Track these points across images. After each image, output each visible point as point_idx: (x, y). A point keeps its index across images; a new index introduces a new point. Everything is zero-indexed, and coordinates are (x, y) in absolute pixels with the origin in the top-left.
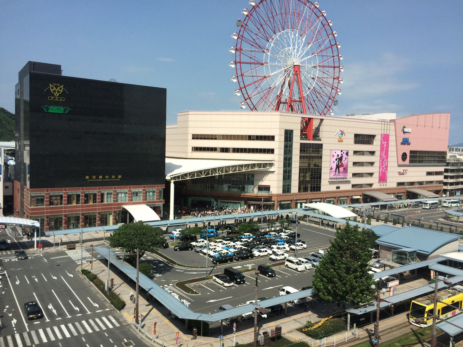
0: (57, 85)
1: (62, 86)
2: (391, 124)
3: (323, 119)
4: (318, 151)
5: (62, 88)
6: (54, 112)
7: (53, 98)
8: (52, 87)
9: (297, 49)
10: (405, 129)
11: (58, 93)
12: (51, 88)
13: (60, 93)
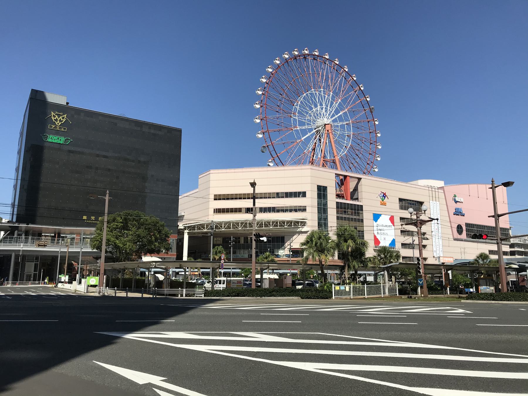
1: (66, 115)
2: (439, 191)
3: (361, 178)
4: (358, 213)
5: (65, 117)
6: (53, 141)
7: (53, 126)
8: (53, 115)
9: (326, 108)
10: (456, 198)
11: (60, 122)
12: (53, 116)
13: (63, 123)
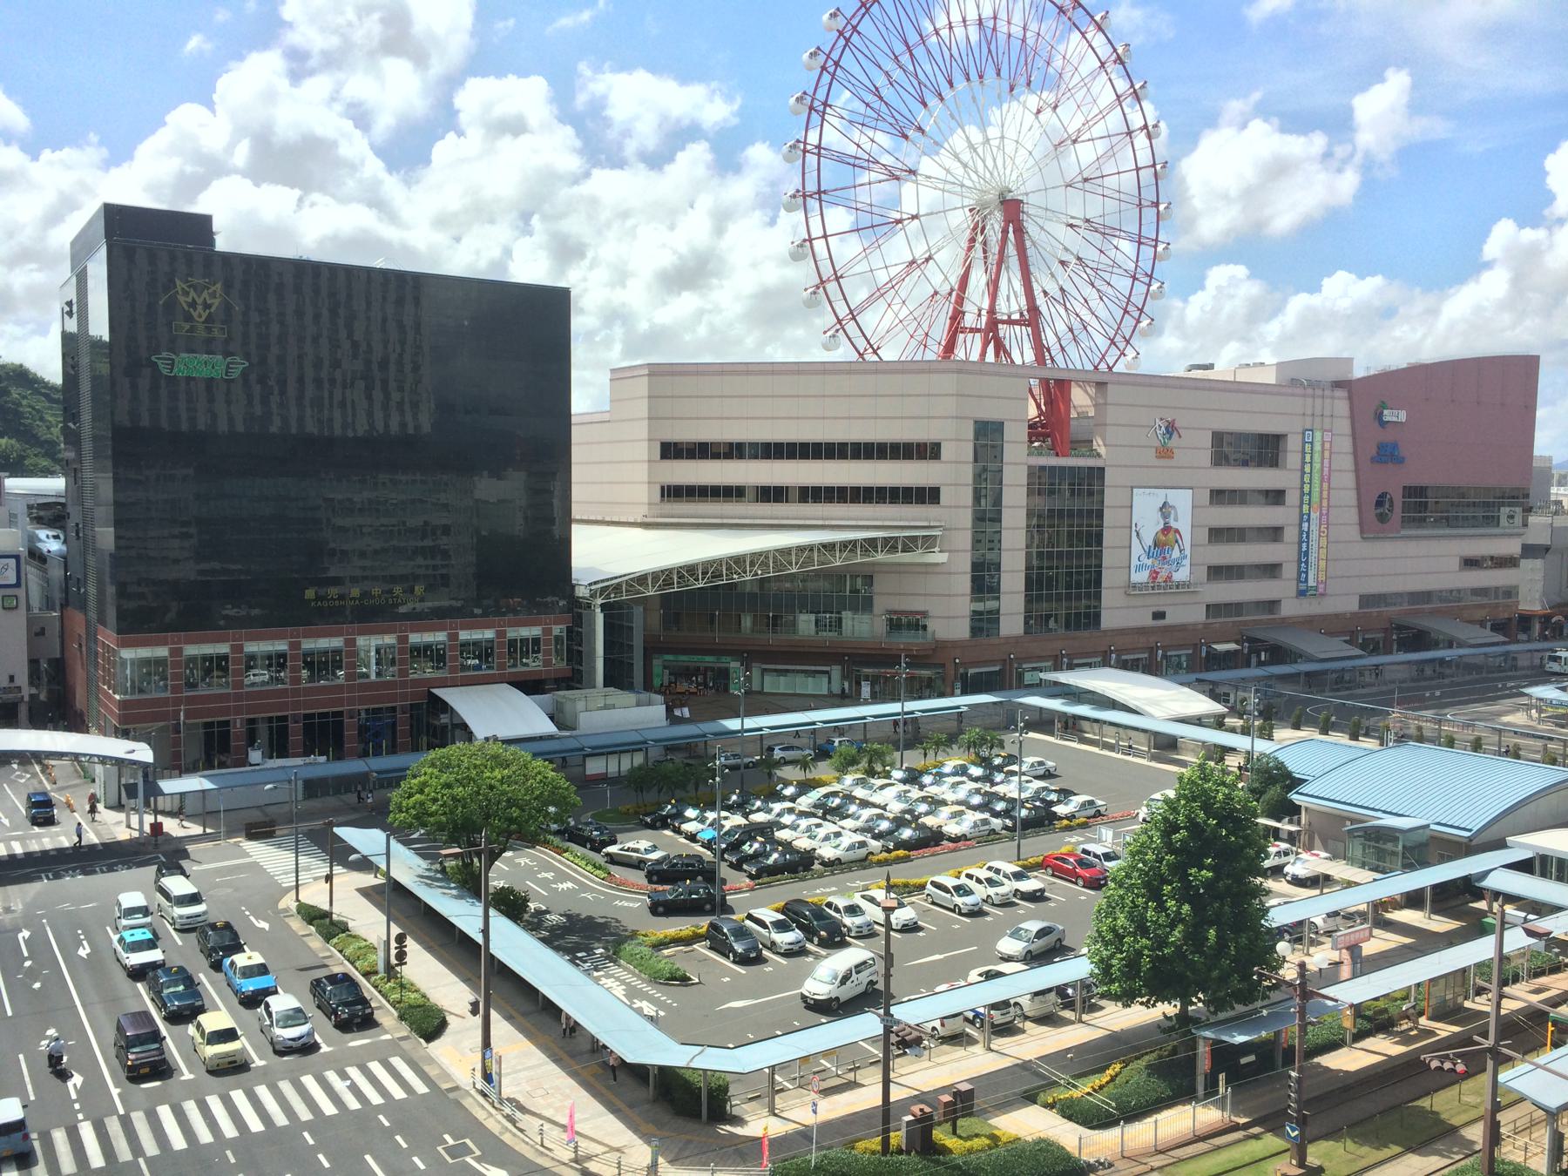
10: (1386, 412)
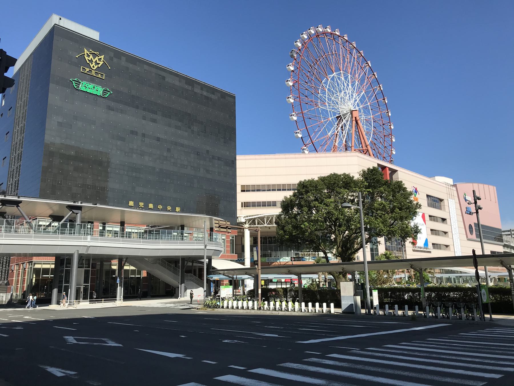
0: (95, 53)
1: (103, 56)
13: (99, 66)
